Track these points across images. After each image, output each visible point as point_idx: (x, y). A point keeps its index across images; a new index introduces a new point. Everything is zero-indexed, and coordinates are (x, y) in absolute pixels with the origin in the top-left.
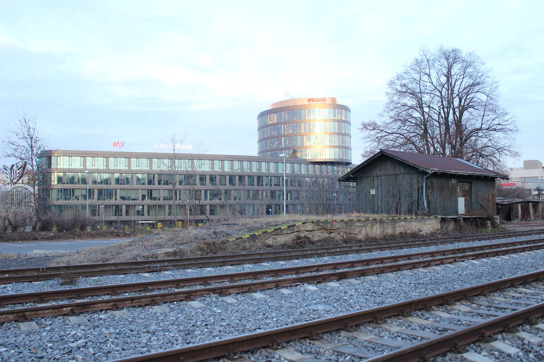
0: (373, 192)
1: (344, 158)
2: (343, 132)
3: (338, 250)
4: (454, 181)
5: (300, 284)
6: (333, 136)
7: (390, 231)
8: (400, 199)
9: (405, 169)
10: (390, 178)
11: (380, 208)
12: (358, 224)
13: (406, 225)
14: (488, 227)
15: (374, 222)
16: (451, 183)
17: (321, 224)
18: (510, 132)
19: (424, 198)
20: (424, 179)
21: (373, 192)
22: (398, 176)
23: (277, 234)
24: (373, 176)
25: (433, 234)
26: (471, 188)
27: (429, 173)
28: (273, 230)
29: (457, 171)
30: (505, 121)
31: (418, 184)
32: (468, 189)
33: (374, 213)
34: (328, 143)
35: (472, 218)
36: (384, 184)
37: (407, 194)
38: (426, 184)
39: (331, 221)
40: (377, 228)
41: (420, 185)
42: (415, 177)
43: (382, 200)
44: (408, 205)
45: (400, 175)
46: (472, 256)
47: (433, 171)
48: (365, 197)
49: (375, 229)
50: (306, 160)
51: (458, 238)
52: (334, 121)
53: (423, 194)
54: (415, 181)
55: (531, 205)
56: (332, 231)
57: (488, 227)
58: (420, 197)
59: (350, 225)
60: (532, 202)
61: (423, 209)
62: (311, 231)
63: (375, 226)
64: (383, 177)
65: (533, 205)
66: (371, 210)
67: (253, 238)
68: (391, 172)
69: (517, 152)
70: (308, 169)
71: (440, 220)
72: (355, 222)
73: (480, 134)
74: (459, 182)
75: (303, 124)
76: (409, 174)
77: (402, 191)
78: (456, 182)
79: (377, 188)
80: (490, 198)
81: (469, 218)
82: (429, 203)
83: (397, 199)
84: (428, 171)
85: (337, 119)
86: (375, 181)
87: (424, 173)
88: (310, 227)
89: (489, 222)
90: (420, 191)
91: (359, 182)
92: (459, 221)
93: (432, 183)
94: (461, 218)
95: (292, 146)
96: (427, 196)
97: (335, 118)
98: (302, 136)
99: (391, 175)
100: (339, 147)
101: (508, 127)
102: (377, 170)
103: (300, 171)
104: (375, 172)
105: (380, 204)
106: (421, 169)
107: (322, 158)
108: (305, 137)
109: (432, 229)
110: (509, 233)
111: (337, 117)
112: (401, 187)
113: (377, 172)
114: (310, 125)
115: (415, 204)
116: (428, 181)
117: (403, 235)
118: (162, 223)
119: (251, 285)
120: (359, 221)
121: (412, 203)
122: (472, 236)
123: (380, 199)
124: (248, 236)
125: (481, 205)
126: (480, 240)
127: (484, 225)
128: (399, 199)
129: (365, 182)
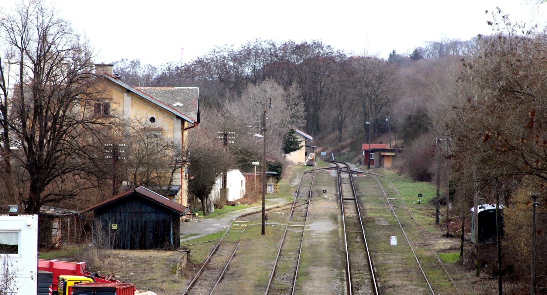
22: (144, 215)
24: (116, 212)
45: (145, 213)
64: (127, 214)
68: (137, 210)
76: (156, 213)
99: (136, 213)
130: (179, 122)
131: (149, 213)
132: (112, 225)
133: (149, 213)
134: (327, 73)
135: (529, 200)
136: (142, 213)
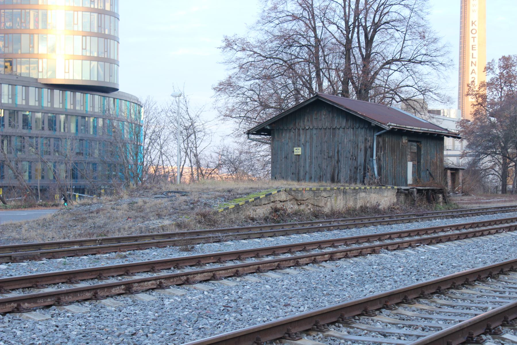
0: (298, 151)
1: (107, 80)
2: (107, 33)
3: (321, 225)
4: (405, 140)
5: (420, 245)
6: (88, 38)
7: (351, 204)
8: (338, 161)
9: (347, 121)
10: (325, 134)
11: (307, 174)
12: (324, 194)
13: (366, 197)
14: (440, 202)
15: (338, 192)
16: (402, 142)
17: (293, 193)
18: (442, 67)
19: (375, 162)
20: (375, 137)
21: (298, 151)
22: (337, 131)
23: (257, 204)
24: (299, 130)
25: (391, 209)
26: (419, 149)
27: (383, 129)
28: (253, 199)
29: (412, 127)
30: (436, 50)
31: (366, 143)
32: (416, 151)
33: (299, 180)
34: (79, 52)
35: (425, 190)
36: (315, 141)
37: (348, 155)
38: (378, 143)
39: (301, 189)
40: (340, 200)
41: (369, 144)
42: (362, 134)
43: (311, 163)
44: (350, 170)
45: (339, 129)
46: (506, 228)
47: (391, 127)
48: (286, 157)
49: (338, 202)
50: (37, 79)
51: (421, 216)
52: (92, 11)
53: (372, 157)
54: (361, 139)
55: (449, 172)
56: (302, 202)
57: (440, 202)
58: (367, 161)
59: (318, 195)
60: (451, 169)
61: (373, 175)
62: (284, 201)
63: (339, 198)
64: (314, 131)
65: (451, 173)
66: (294, 176)
67: (238, 209)
68: (327, 125)
69: (449, 97)
70: (40, 99)
71: (397, 191)
72: (321, 191)
73: (393, 67)
74: (409, 141)
75: (32, 13)
76: (353, 128)
77: (342, 152)
78: (406, 141)
79: (304, 145)
80: (438, 163)
81: (422, 190)
82: (380, 169)
83: (334, 162)
84: (384, 126)
85: (96, 7)
86: (301, 136)
87: (378, 128)
88: (283, 196)
89: (441, 196)
90: (369, 152)
91: (276, 136)
92: (412, 193)
93: (384, 141)
94: (415, 190)
95: (11, 51)
96: (379, 160)
97: (92, 6)
98: (31, 34)
99: (326, 129)
100: (98, 59)
101: (440, 59)
102: (306, 121)
103: (27, 99)
104: (301, 124)
105: (307, 168)
106: (374, 124)
107: (67, 78)
108: (36, 36)
109: (389, 203)
110: (461, 211)
111: (96, 4)
112: (340, 145)
113: (305, 123)
114: (45, 15)
115: (360, 170)
116: (381, 140)
117: (364, 209)
118: (3, 189)
119: (316, 256)
120: (325, 190)
121: (356, 168)
122: (433, 214)
123: (308, 161)
124: (233, 206)
125: (430, 173)
126: (286, 233)
127: (435, 199)
128: (337, 162)
129: (286, 137)
130: (389, 77)
131: (344, 128)
132: (295, 148)
133: (344, 128)
134: (163, 333)
135: (366, 67)
136: (334, 129)
